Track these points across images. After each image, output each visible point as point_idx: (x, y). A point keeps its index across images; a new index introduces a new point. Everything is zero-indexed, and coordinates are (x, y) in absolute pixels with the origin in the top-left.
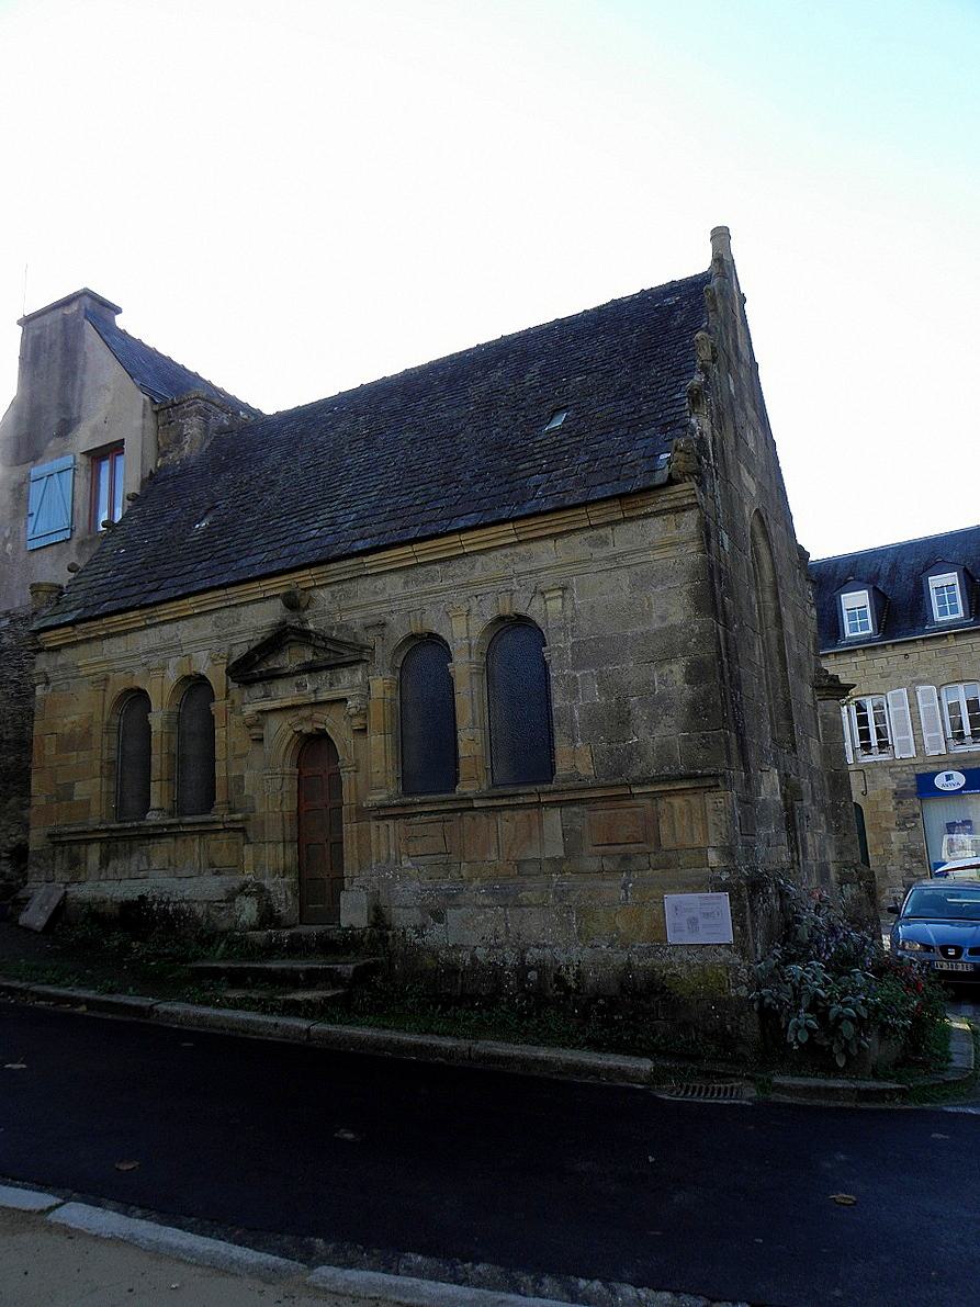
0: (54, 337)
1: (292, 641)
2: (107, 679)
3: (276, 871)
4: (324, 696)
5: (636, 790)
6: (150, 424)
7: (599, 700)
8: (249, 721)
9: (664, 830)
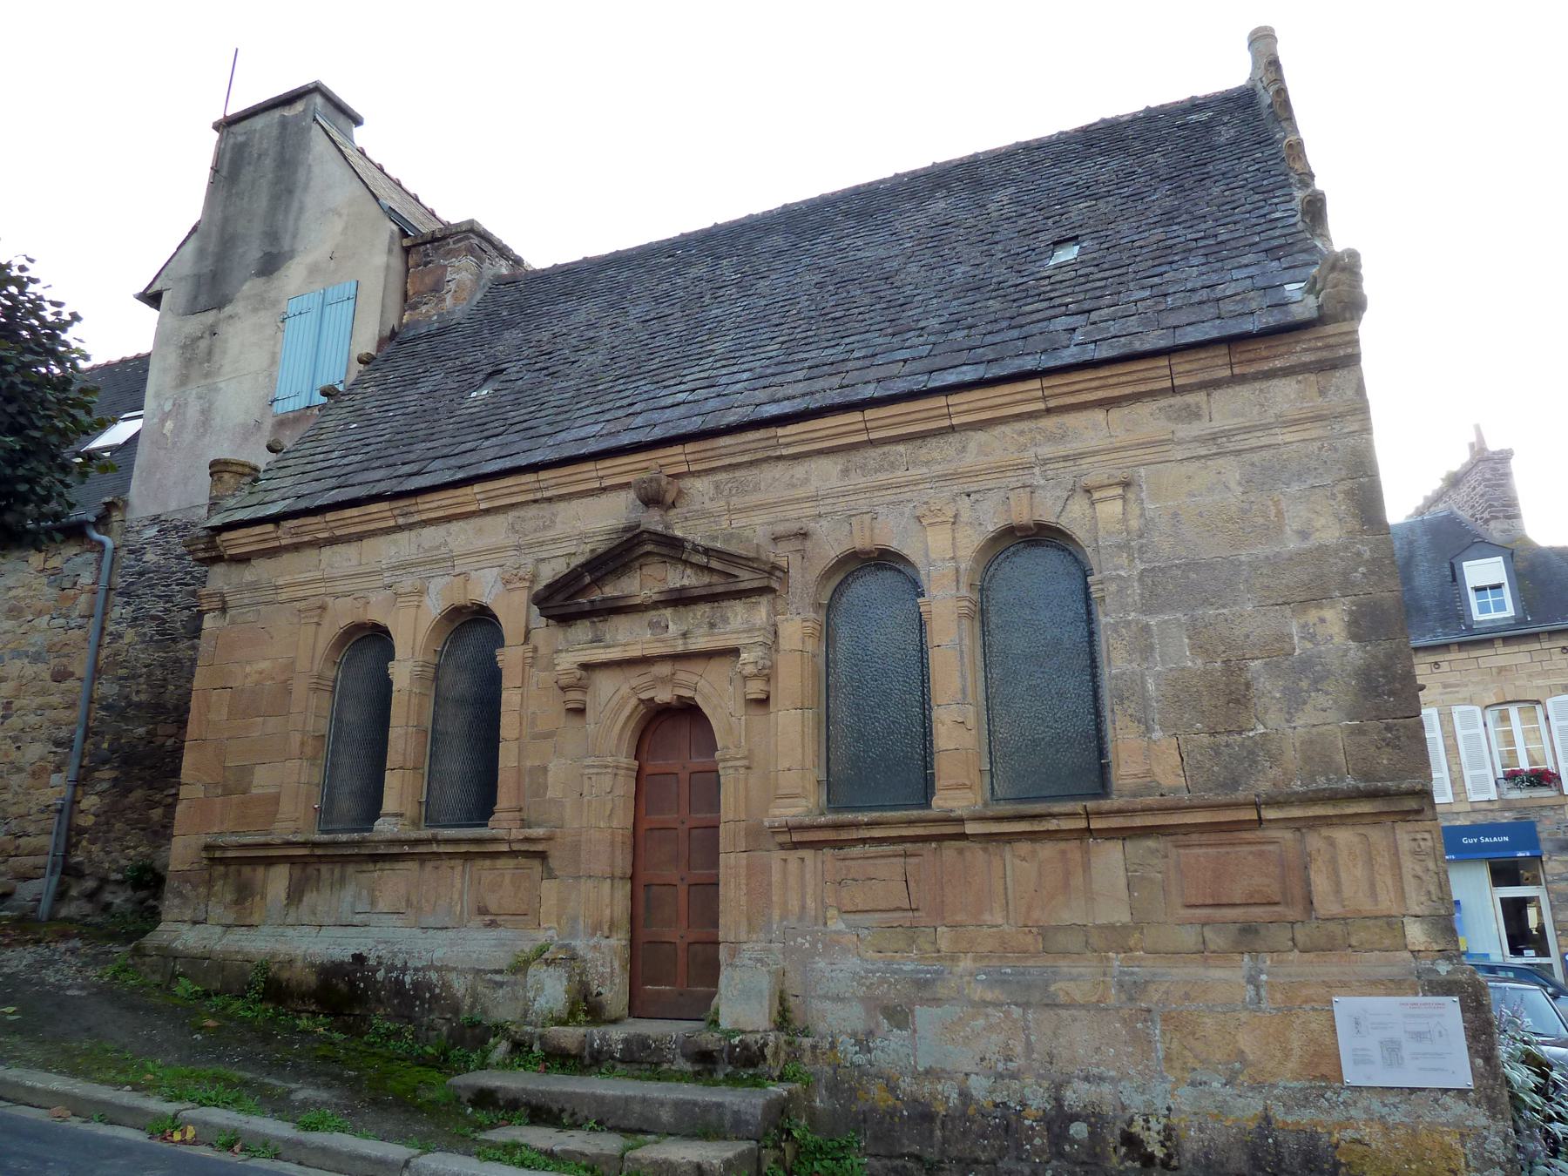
0: (265, 146)
1: (648, 554)
2: (323, 608)
3: (596, 928)
4: (700, 643)
5: (1269, 814)
6: (397, 262)
7: (1193, 663)
8: (564, 681)
9: (1320, 883)
